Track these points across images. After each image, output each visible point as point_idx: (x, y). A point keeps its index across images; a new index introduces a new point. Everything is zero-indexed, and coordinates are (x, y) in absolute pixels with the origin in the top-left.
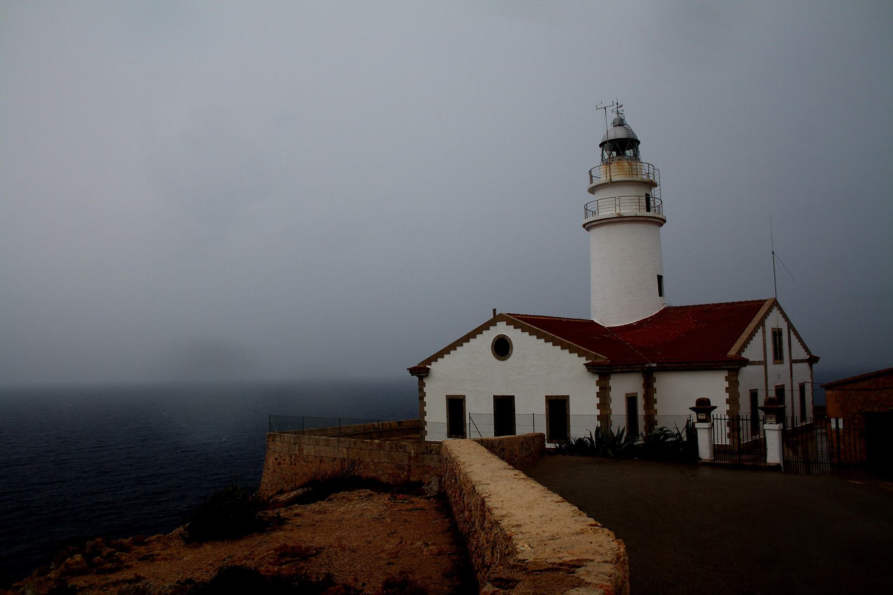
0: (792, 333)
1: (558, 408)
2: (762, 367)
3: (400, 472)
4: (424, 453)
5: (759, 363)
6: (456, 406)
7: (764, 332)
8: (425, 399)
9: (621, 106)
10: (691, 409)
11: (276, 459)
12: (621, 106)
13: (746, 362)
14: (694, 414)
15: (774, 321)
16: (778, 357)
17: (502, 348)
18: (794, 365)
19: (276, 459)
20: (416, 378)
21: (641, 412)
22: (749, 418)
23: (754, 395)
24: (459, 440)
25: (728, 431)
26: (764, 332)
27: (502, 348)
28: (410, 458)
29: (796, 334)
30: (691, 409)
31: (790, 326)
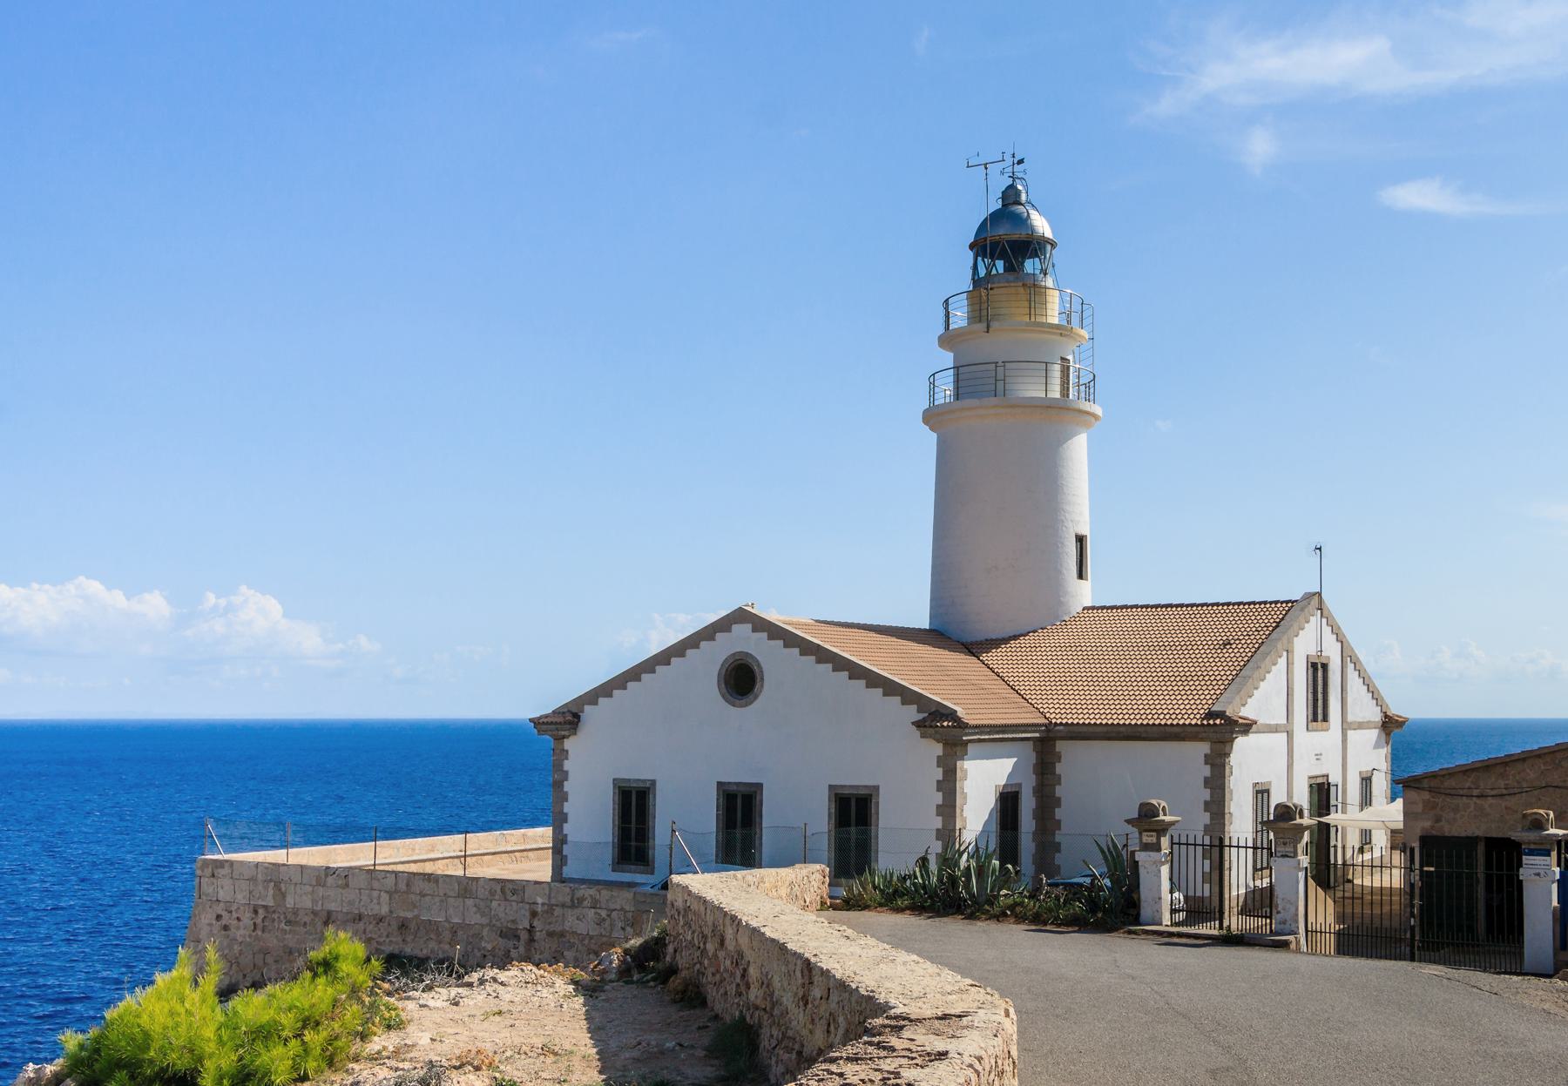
0: (1350, 666)
2: (1350, 718)
3: (510, 944)
4: (563, 906)
5: (1274, 729)
7: (1289, 664)
8: (567, 786)
9: (1021, 162)
10: (1128, 821)
11: (219, 917)
12: (1021, 162)
13: (1247, 727)
14: (1133, 831)
15: (1307, 640)
16: (1318, 713)
18: (1350, 733)
19: (219, 917)
20: (547, 738)
22: (1250, 844)
23: (1262, 793)
24: (740, 874)
25: (1207, 869)
26: (1289, 664)
28: (534, 914)
29: (1356, 663)
30: (1128, 821)
31: (1348, 655)
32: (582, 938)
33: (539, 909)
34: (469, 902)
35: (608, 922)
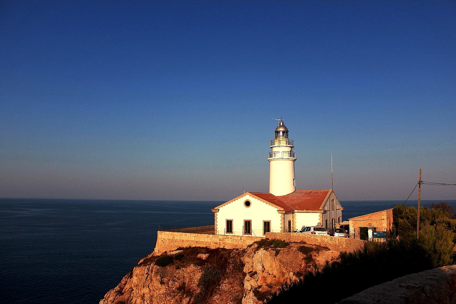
1: (267, 225)
5: (338, 209)
6: (229, 224)
17: (248, 204)
21: (292, 226)
27: (248, 204)
28: (220, 240)
32: (229, 243)
33: (221, 239)
34: (209, 238)
35: (233, 241)
